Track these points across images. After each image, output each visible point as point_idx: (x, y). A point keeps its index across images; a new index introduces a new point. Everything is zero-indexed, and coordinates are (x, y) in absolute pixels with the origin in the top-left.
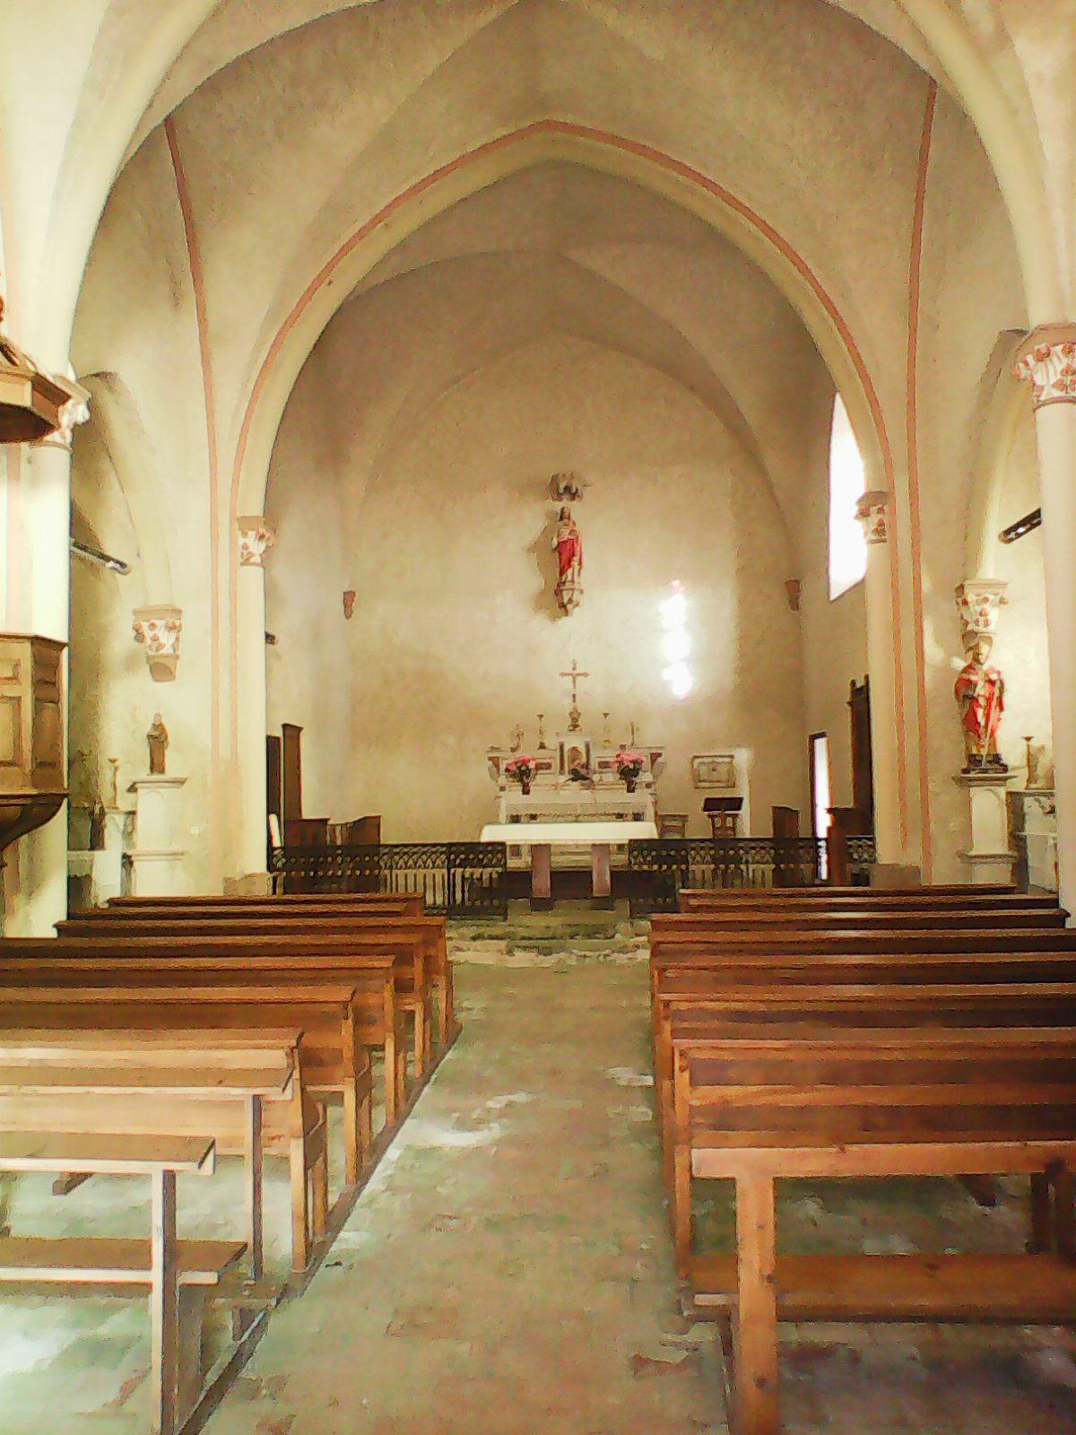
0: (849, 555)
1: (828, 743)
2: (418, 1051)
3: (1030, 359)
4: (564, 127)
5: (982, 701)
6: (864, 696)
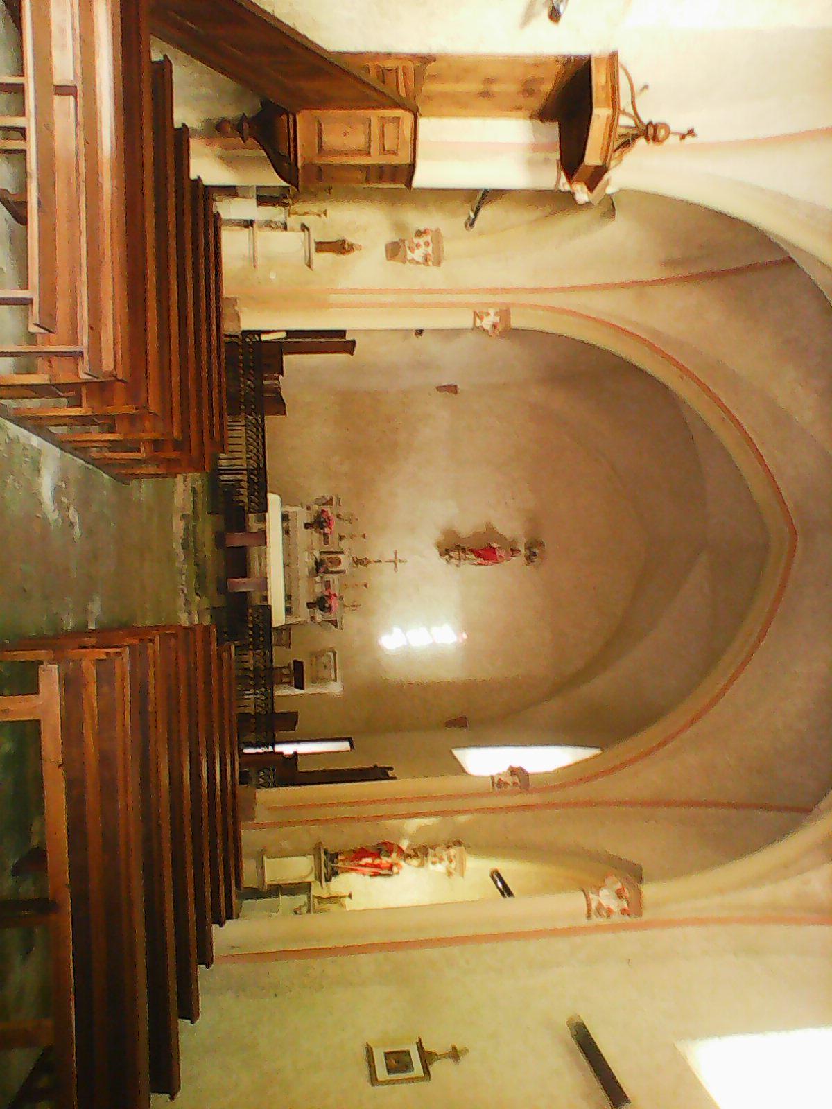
0: (484, 762)
1: (348, 751)
2: (109, 455)
3: (619, 886)
4: (793, 550)
5: (377, 861)
6: (382, 776)
